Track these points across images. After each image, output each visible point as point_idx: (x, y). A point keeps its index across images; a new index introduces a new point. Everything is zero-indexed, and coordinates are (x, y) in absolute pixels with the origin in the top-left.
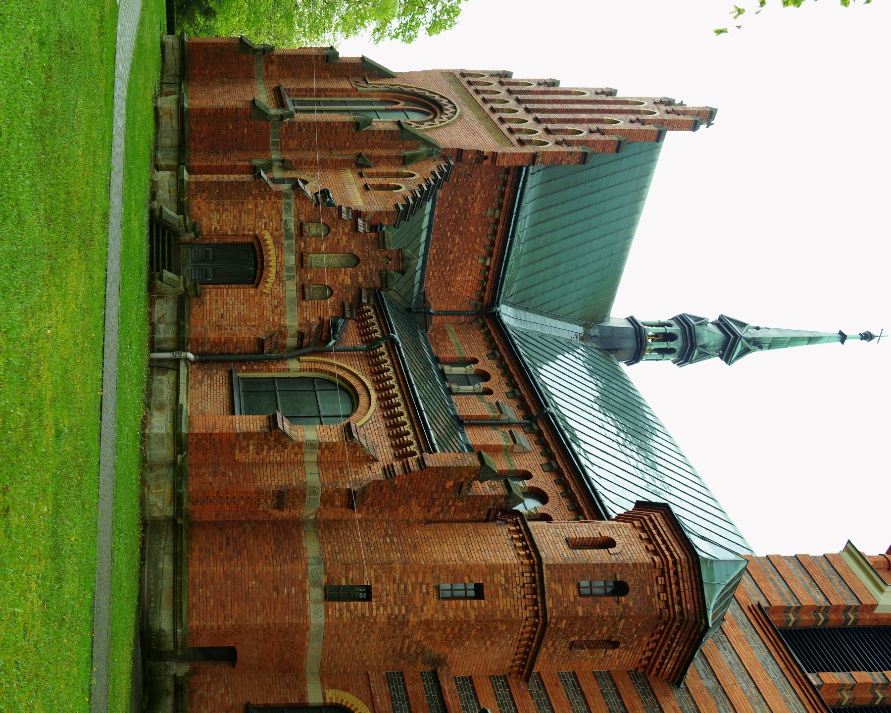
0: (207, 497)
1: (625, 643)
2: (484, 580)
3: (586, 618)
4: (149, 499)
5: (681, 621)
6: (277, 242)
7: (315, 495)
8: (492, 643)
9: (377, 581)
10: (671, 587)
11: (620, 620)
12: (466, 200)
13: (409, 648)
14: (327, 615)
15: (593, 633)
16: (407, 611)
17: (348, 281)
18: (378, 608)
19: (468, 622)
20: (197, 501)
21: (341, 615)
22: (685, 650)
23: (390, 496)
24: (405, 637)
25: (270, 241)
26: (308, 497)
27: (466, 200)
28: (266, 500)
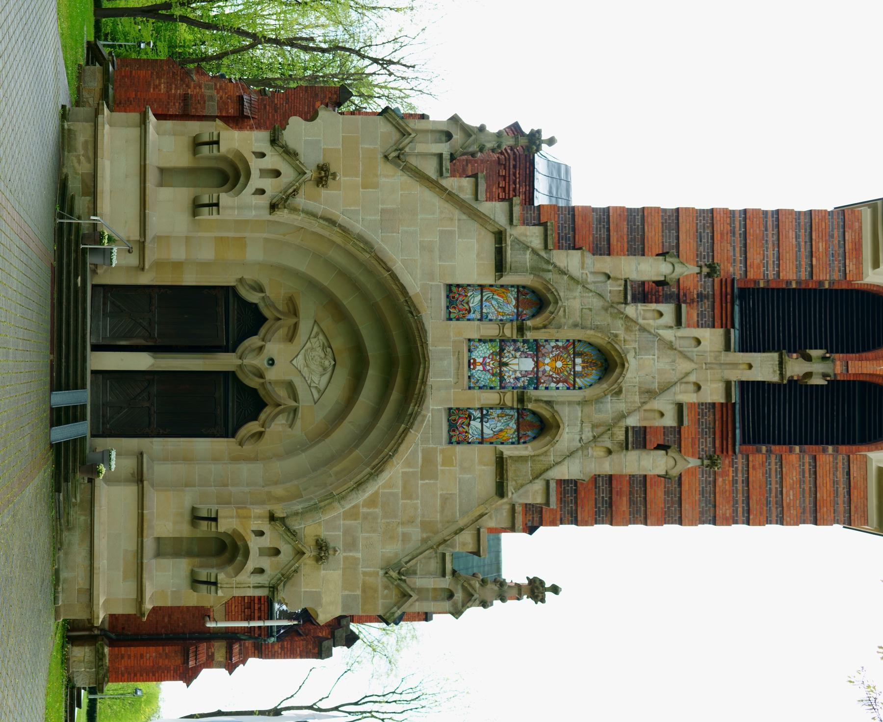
0: (128, 98)
4: (83, 96)
5: (515, 159)
7: (212, 101)
10: (509, 176)
11: (467, 165)
20: (120, 103)
22: (528, 189)
23: (273, 116)
26: (207, 103)
28: (174, 104)
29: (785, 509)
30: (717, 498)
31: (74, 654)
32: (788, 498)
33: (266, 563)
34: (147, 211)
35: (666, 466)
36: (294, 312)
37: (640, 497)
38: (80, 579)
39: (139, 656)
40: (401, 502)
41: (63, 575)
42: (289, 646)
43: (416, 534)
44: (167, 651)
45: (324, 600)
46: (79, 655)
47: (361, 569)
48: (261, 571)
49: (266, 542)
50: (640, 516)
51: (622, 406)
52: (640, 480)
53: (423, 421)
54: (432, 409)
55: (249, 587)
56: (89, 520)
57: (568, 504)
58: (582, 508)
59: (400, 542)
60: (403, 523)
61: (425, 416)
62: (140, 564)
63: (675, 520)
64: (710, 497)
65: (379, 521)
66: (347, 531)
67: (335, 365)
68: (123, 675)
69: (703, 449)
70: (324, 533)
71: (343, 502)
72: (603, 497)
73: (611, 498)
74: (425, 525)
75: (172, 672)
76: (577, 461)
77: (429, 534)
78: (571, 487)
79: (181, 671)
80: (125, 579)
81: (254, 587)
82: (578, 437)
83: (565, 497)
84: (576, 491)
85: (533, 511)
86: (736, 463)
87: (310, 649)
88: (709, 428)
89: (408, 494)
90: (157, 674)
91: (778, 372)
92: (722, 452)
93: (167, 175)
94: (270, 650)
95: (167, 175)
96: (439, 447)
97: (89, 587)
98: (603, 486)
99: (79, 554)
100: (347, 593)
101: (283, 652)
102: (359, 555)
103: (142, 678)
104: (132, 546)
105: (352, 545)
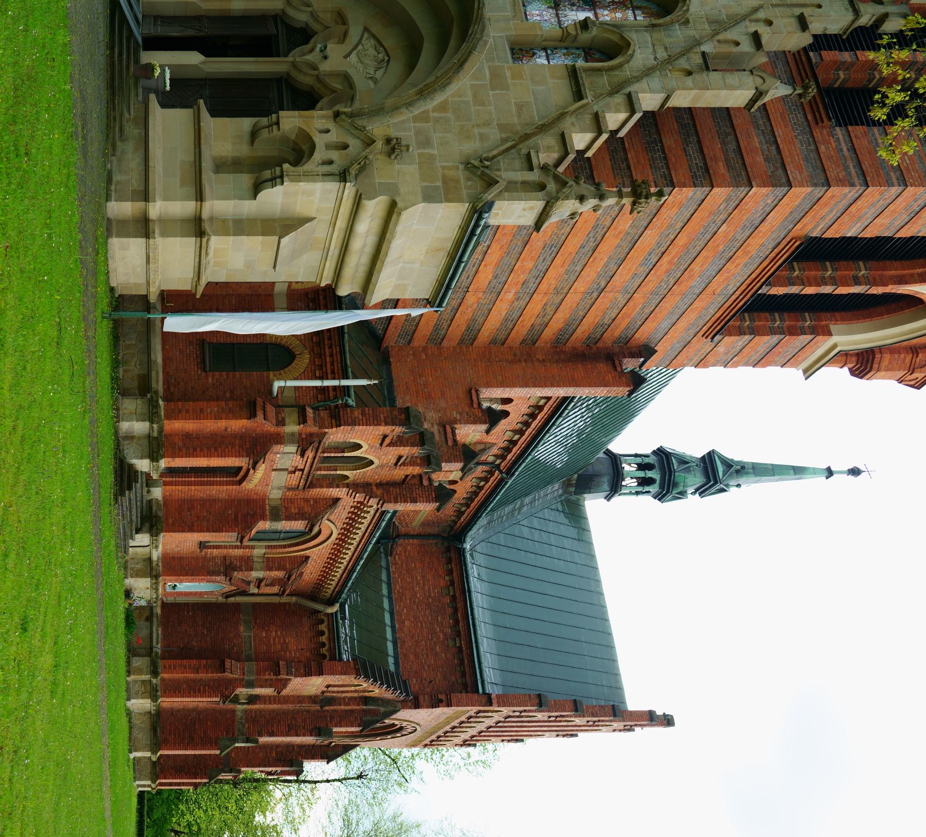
29: (904, 172)
30: (824, 163)
31: (124, 406)
32: (904, 163)
33: (334, 155)
34: (202, 124)
35: (755, 84)
36: (344, 21)
37: (738, 163)
38: (134, 182)
39: (198, 411)
40: (473, 108)
41: (116, 177)
42: (371, 412)
43: (494, 135)
44: (231, 406)
45: (401, 189)
46: (130, 407)
47: (439, 165)
48: (330, 162)
49: (335, 136)
50: (743, 180)
51: (691, 32)
52: (734, 149)
53: (485, 45)
54: (493, 36)
55: (318, 175)
56: (143, 133)
57: (660, 169)
58: (675, 171)
59: (478, 141)
60: (478, 126)
61: (486, 42)
62: (198, 171)
63: (783, 183)
64: (816, 162)
65: (453, 123)
66: (418, 132)
67: (389, 61)
68: (180, 450)
69: (795, 123)
70: (393, 133)
71: (411, 109)
72: (696, 164)
73: (706, 164)
74: (502, 127)
75: (237, 447)
76: (657, 80)
77: (508, 135)
78: (660, 155)
79: (248, 446)
80: (183, 184)
81: (323, 175)
82: (653, 57)
83: (654, 163)
84: (665, 158)
85: (622, 175)
86: (836, 134)
87: (396, 416)
88: (797, 106)
89: (479, 101)
90: (220, 450)
91: (851, 10)
92: (817, 124)
93: (221, 166)
94: (349, 415)
95: (221, 166)
96: (506, 65)
97: (143, 188)
98: (693, 153)
99: (133, 161)
100: (426, 184)
101: (364, 418)
102: (435, 152)
103: (202, 453)
104: (190, 157)
105: (426, 142)
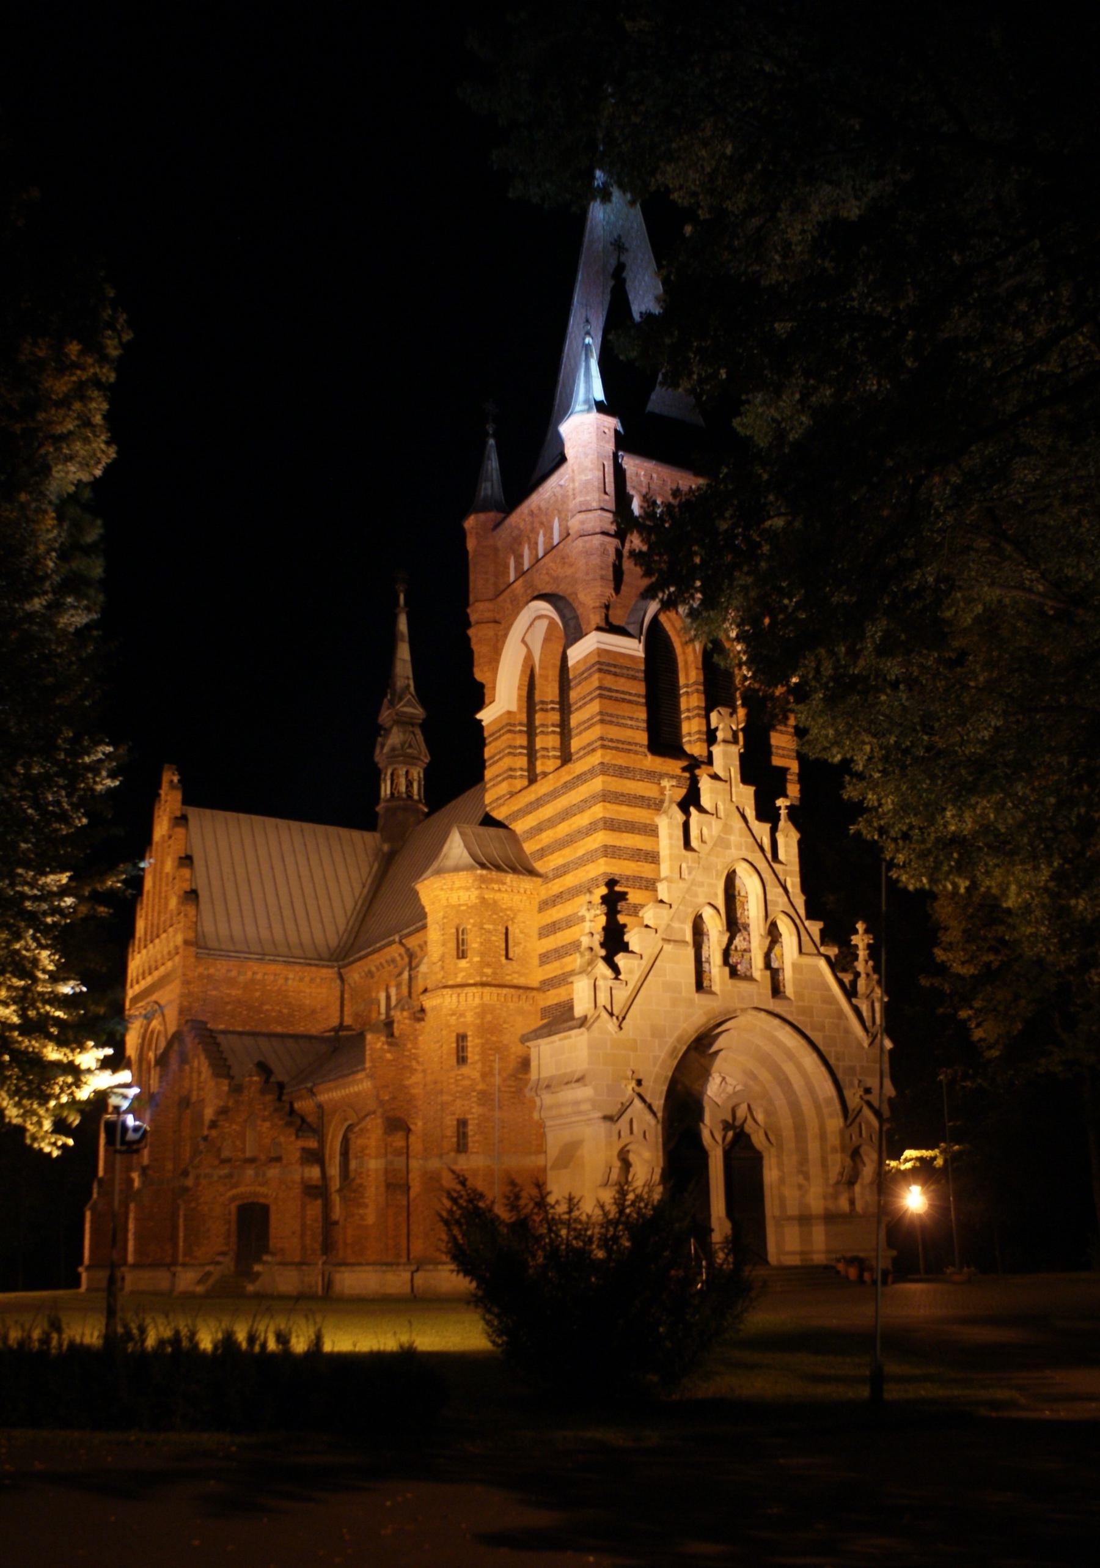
1: (508, 920)
2: (454, 1031)
3: (482, 955)
6: (235, 1186)
8: (505, 1022)
9: (454, 1114)
12: (228, 1003)
13: (510, 1086)
14: (477, 1153)
15: (498, 947)
16: (475, 1091)
17: (268, 1124)
18: (472, 1113)
19: (483, 1045)
21: (477, 1141)
24: (500, 1091)
25: (234, 1192)
27: (228, 1003)
